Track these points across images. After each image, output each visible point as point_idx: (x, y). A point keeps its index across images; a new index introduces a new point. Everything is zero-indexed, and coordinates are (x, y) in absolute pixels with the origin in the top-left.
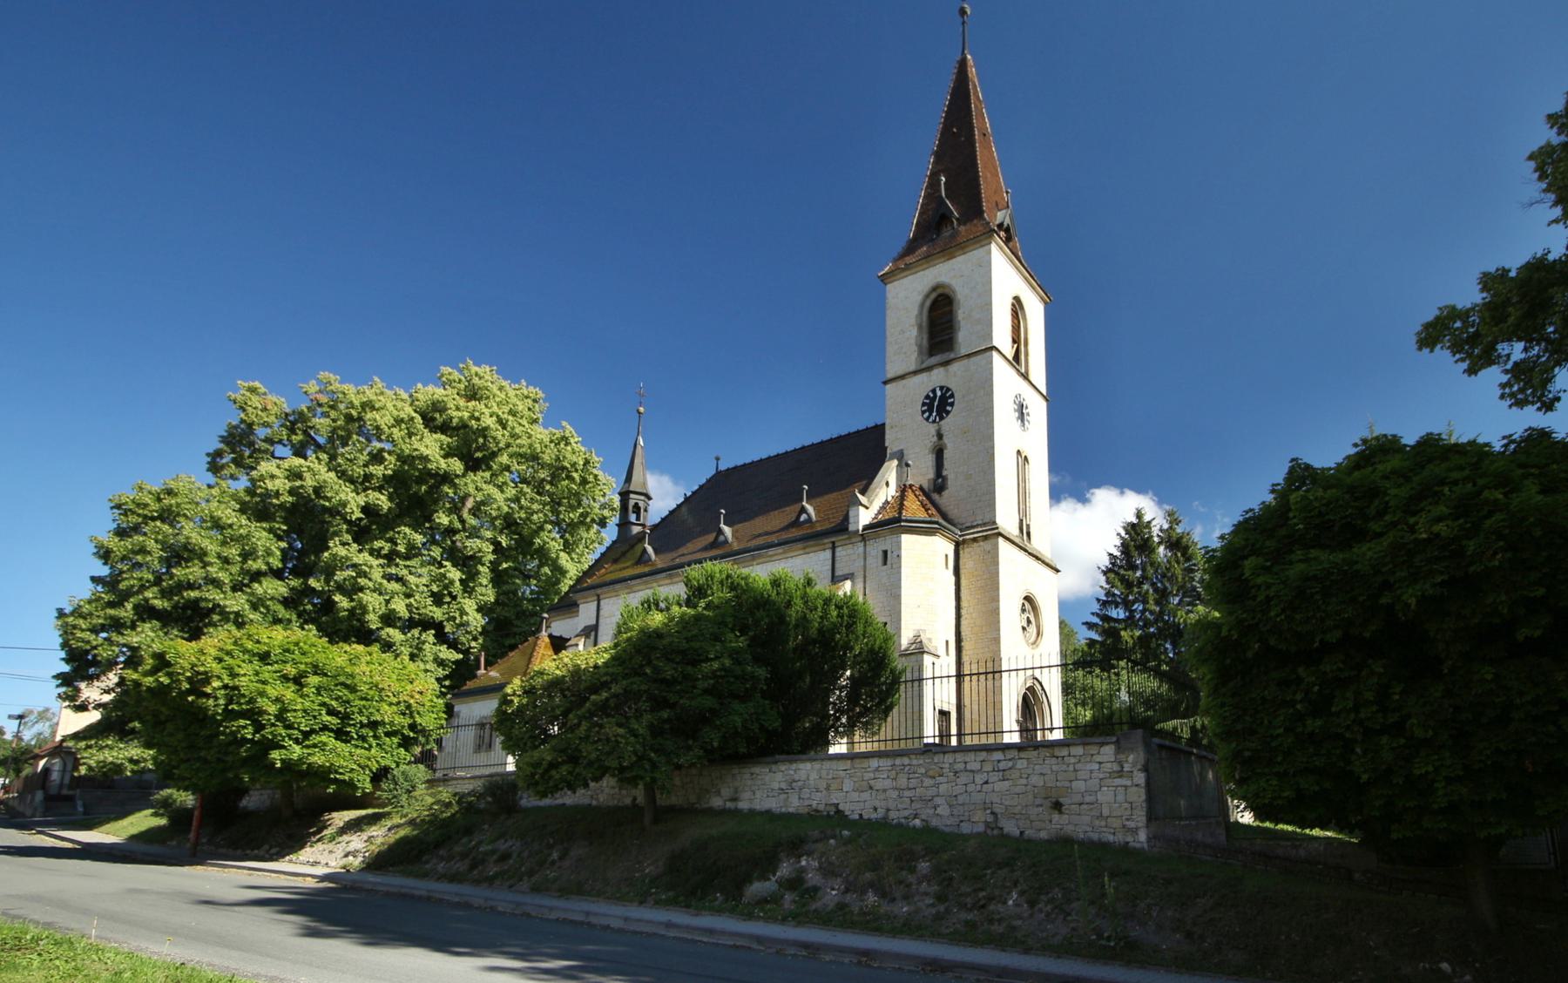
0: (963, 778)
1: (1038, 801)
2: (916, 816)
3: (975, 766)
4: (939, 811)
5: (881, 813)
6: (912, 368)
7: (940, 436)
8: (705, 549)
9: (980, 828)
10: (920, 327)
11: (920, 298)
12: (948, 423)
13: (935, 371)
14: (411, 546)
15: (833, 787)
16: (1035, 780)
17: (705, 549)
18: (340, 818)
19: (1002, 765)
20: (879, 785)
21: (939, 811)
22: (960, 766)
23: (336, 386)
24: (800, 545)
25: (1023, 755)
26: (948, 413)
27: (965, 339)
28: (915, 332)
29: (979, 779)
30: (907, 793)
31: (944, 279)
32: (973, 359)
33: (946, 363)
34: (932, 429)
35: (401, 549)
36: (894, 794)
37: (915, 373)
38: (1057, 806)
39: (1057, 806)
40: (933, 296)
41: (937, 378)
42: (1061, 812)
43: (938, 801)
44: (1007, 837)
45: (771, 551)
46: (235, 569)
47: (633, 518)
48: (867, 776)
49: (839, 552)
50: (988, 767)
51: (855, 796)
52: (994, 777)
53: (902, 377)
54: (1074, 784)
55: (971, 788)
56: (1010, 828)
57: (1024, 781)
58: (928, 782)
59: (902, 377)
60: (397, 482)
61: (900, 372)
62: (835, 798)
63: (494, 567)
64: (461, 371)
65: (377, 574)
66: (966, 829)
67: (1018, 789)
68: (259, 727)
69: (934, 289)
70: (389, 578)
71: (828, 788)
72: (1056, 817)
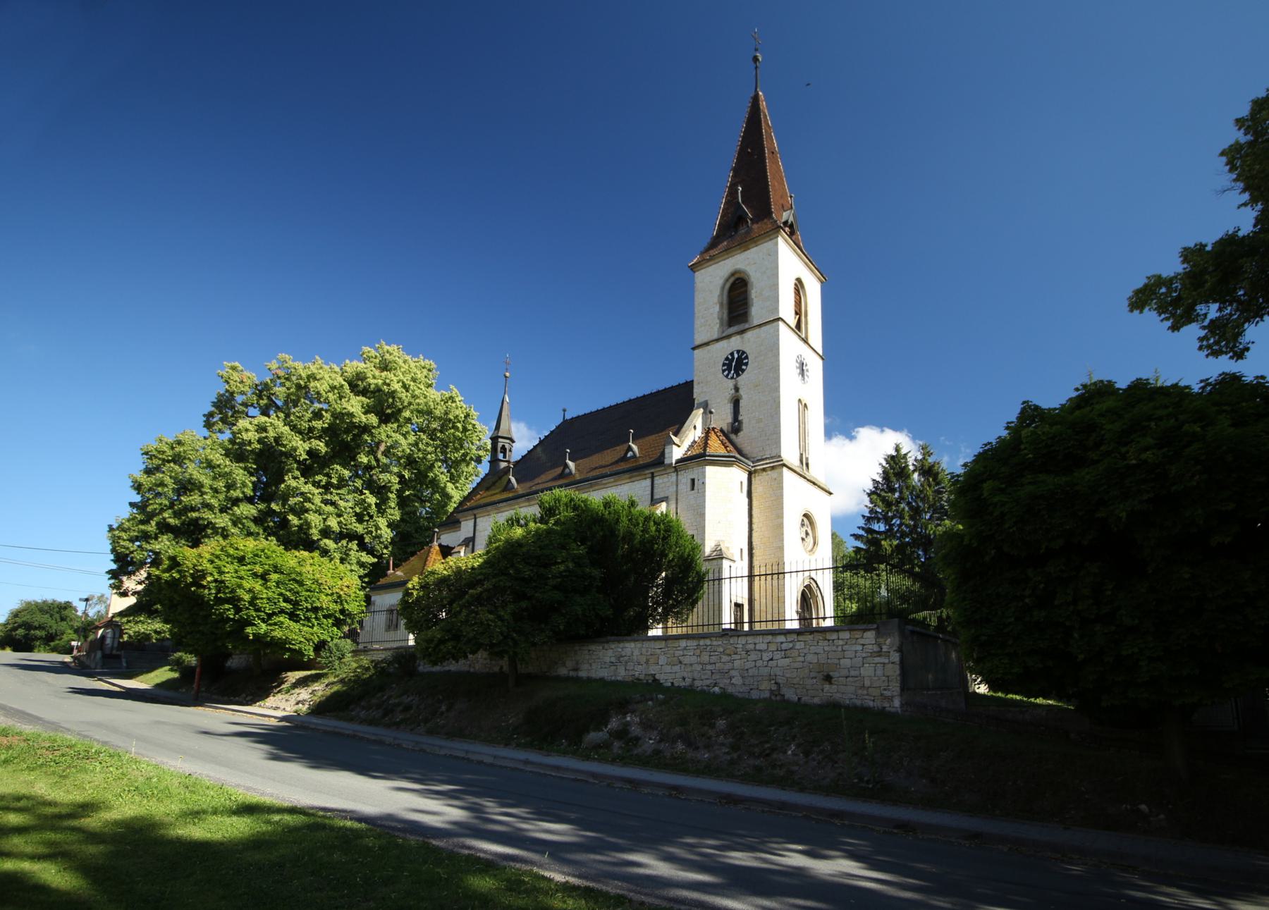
0: (753, 656)
1: (813, 674)
2: (715, 685)
3: (763, 647)
4: (734, 681)
5: (688, 682)
6: (715, 336)
7: (737, 389)
8: (554, 479)
9: (767, 695)
10: (721, 305)
11: (721, 282)
12: (743, 379)
13: (733, 339)
14: (341, 479)
15: (652, 661)
16: (810, 658)
17: (554, 479)
18: (294, 676)
19: (784, 646)
20: (686, 660)
21: (734, 681)
22: (752, 647)
23: (290, 363)
24: (627, 476)
25: (801, 638)
26: (743, 371)
27: (757, 313)
28: (717, 308)
29: (766, 656)
30: (709, 667)
31: (740, 266)
32: (764, 328)
33: (742, 332)
34: (731, 383)
35: (334, 481)
36: (699, 668)
37: (717, 340)
38: (828, 679)
39: (828, 679)
40: (732, 280)
41: (735, 344)
42: (831, 683)
43: (733, 673)
44: (788, 702)
45: (605, 481)
46: (222, 497)
47: (501, 456)
48: (678, 653)
49: (658, 480)
50: (773, 647)
51: (668, 669)
52: (778, 655)
53: (707, 344)
54: (842, 661)
55: (759, 663)
56: (791, 695)
57: (801, 659)
58: (725, 658)
59: (707, 344)
60: (330, 433)
61: (706, 340)
62: (653, 670)
63: (400, 493)
64: (376, 350)
65: (317, 500)
66: (755, 695)
67: (796, 665)
68: (238, 610)
69: (733, 274)
70: (326, 502)
71: (647, 662)
72: (827, 687)
